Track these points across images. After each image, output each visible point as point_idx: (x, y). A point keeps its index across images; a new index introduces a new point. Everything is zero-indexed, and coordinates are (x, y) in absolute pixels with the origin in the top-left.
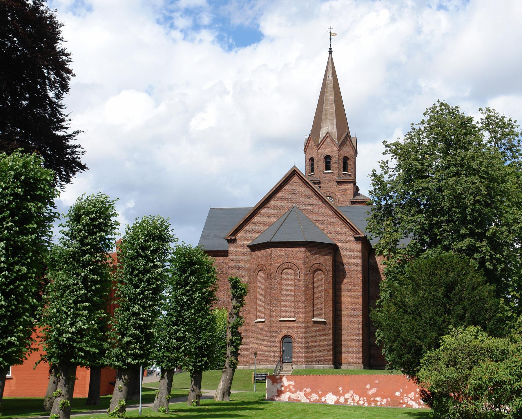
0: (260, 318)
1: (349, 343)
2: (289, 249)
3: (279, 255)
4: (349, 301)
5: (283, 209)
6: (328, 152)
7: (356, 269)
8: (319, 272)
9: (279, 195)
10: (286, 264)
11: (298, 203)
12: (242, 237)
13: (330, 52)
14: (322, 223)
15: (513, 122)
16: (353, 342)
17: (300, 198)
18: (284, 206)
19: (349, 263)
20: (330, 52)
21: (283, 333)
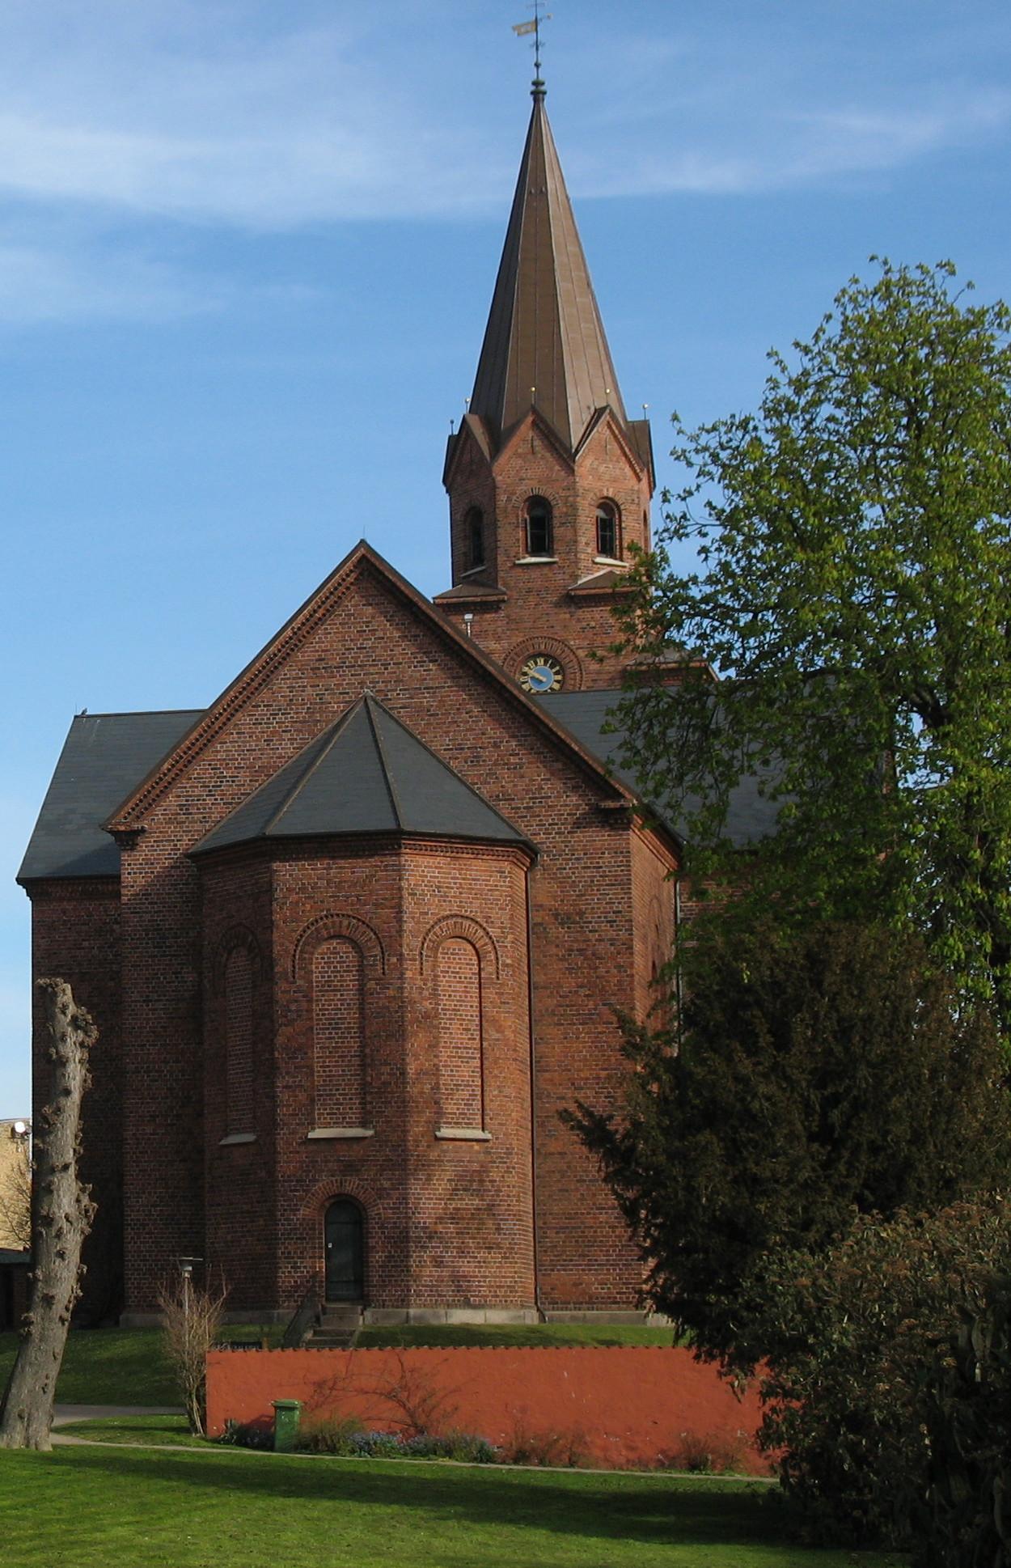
0: (238, 1131)
1: (589, 1222)
2: (342, 863)
3: (303, 889)
4: (585, 1059)
5: (321, 711)
6: (534, 484)
7: (612, 934)
8: (344, 948)
9: (306, 655)
10: (329, 921)
11: (381, 686)
12: (170, 821)
13: (538, 95)
14: (476, 760)
15: (854, 288)
16: (603, 1217)
17: (386, 666)
18: (327, 698)
19: (581, 914)
20: (538, 95)
21: (324, 1185)
